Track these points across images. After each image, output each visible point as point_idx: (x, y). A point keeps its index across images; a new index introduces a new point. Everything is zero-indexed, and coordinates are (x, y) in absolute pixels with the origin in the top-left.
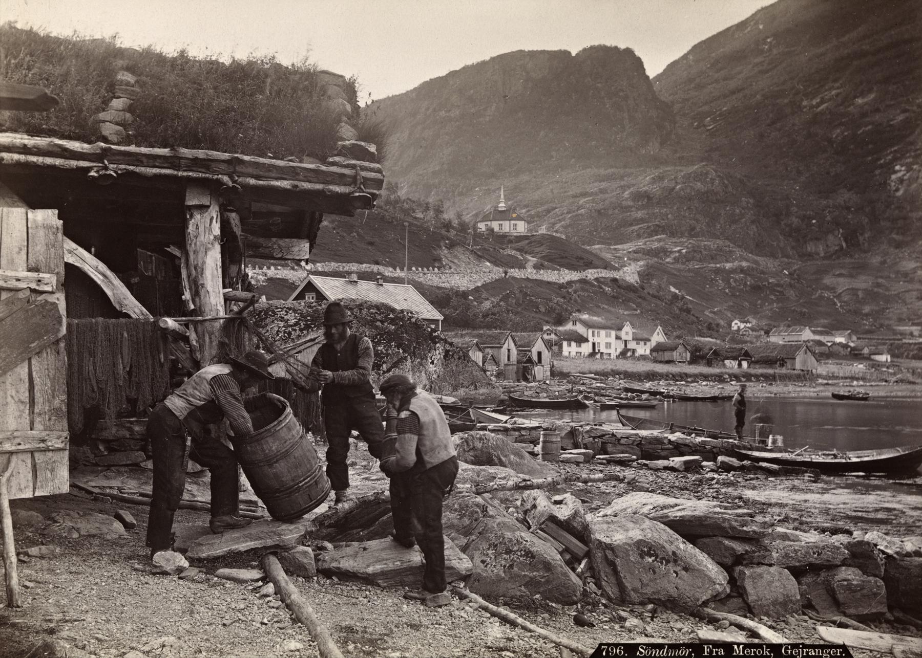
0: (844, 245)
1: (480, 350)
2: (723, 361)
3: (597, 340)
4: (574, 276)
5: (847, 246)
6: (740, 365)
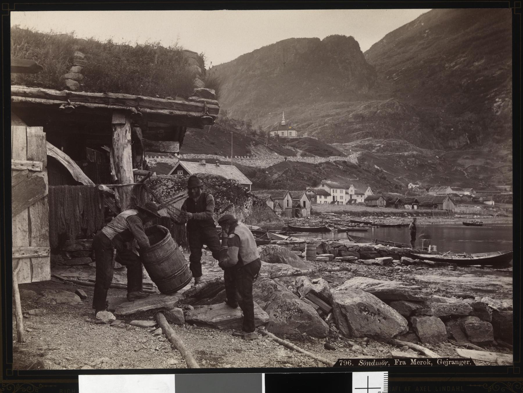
1: (272, 201)
2: (404, 205)
3: (335, 194)
4: (323, 160)
6: (413, 207)
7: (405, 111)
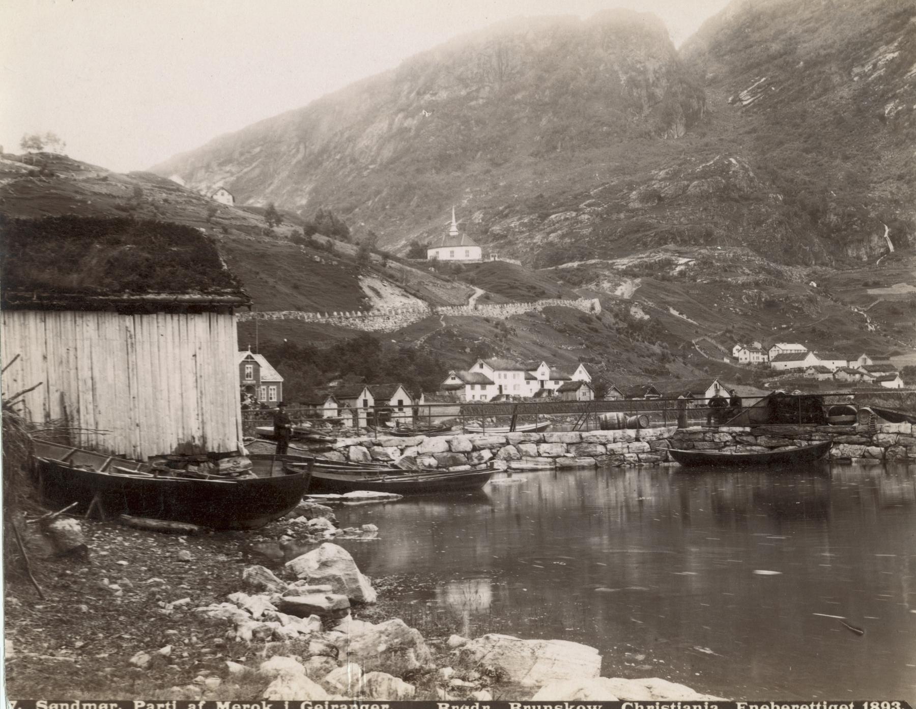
0: (891, 247)
3: (503, 382)
4: (521, 309)
5: (895, 248)
7: (751, 180)
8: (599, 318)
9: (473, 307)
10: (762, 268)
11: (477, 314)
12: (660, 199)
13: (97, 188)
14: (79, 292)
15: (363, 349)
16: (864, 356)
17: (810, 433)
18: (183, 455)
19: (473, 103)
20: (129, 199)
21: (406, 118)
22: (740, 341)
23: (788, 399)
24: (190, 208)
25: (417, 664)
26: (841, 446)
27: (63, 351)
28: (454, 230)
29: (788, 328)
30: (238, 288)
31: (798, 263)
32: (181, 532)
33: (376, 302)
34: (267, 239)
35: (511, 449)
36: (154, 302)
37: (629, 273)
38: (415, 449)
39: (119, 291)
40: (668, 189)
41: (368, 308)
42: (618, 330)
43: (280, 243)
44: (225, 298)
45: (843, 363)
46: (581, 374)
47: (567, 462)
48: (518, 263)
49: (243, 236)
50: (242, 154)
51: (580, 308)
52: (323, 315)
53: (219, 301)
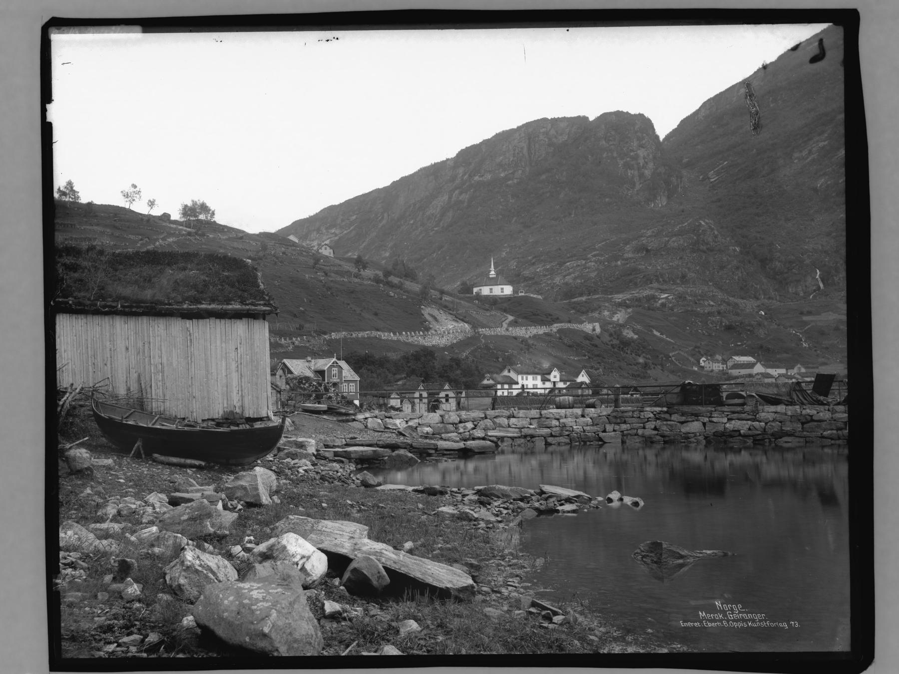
0: (821, 285)
3: (525, 382)
4: (541, 330)
7: (716, 237)
8: (598, 337)
9: (505, 328)
10: (723, 301)
11: (508, 333)
12: (648, 251)
13: (235, 245)
14: (152, 303)
15: (423, 358)
16: (799, 366)
17: (711, 412)
18: (227, 419)
19: (510, 182)
20: (258, 252)
21: (461, 193)
22: (706, 354)
23: (694, 387)
24: (301, 258)
25: (212, 530)
26: (733, 422)
27: (140, 344)
28: (493, 273)
29: (742, 345)
30: (269, 300)
31: (750, 297)
32: (191, 466)
33: (434, 325)
34: (356, 280)
35: (488, 422)
36: (206, 310)
37: (623, 305)
38: (416, 421)
39: (181, 303)
40: (653, 245)
41: (428, 329)
42: (612, 345)
43: (365, 282)
44: (259, 308)
45: (783, 371)
46: (583, 378)
47: (530, 432)
48: (540, 297)
49: (339, 279)
50: (343, 221)
51: (585, 329)
52: (395, 334)
53: (253, 310)
